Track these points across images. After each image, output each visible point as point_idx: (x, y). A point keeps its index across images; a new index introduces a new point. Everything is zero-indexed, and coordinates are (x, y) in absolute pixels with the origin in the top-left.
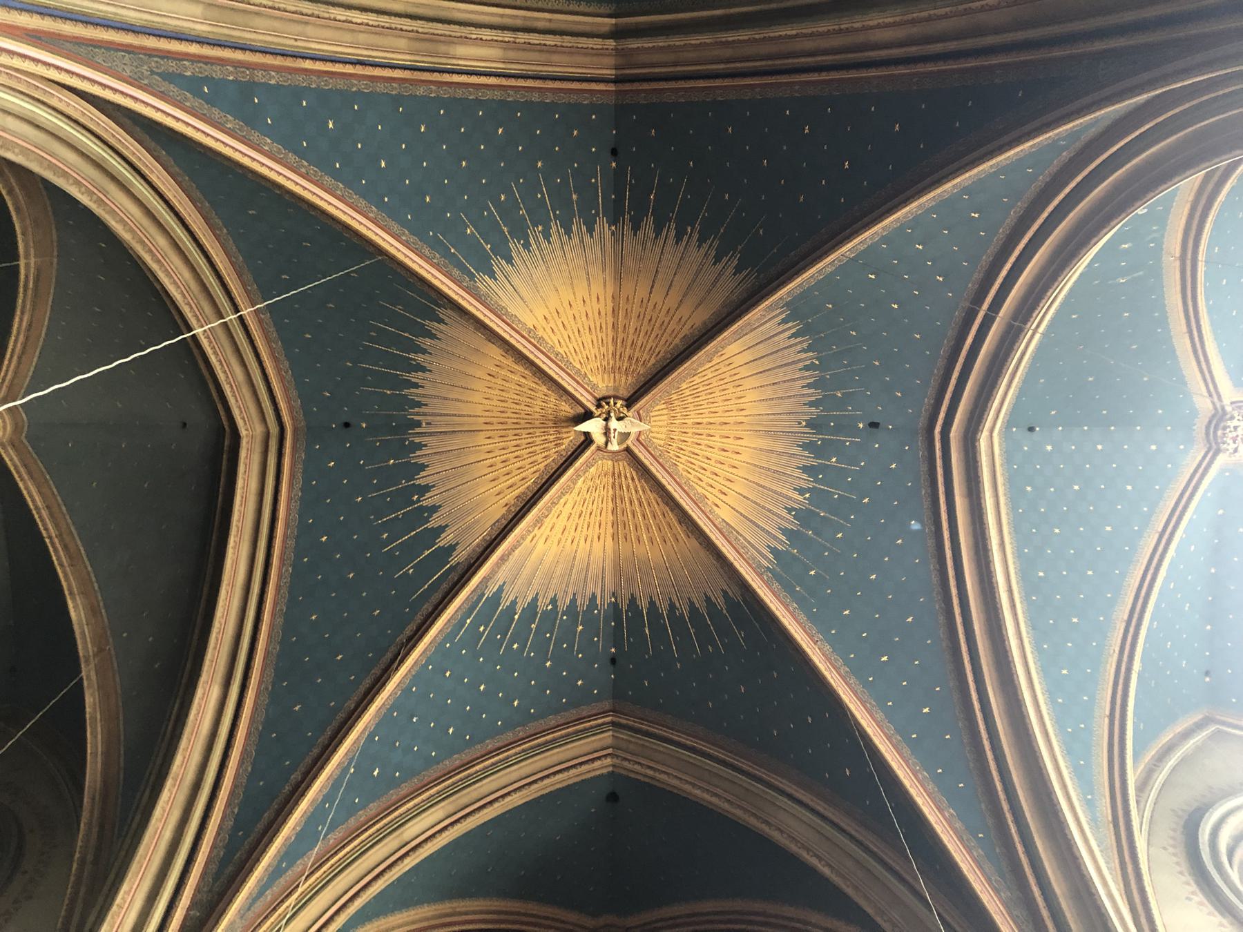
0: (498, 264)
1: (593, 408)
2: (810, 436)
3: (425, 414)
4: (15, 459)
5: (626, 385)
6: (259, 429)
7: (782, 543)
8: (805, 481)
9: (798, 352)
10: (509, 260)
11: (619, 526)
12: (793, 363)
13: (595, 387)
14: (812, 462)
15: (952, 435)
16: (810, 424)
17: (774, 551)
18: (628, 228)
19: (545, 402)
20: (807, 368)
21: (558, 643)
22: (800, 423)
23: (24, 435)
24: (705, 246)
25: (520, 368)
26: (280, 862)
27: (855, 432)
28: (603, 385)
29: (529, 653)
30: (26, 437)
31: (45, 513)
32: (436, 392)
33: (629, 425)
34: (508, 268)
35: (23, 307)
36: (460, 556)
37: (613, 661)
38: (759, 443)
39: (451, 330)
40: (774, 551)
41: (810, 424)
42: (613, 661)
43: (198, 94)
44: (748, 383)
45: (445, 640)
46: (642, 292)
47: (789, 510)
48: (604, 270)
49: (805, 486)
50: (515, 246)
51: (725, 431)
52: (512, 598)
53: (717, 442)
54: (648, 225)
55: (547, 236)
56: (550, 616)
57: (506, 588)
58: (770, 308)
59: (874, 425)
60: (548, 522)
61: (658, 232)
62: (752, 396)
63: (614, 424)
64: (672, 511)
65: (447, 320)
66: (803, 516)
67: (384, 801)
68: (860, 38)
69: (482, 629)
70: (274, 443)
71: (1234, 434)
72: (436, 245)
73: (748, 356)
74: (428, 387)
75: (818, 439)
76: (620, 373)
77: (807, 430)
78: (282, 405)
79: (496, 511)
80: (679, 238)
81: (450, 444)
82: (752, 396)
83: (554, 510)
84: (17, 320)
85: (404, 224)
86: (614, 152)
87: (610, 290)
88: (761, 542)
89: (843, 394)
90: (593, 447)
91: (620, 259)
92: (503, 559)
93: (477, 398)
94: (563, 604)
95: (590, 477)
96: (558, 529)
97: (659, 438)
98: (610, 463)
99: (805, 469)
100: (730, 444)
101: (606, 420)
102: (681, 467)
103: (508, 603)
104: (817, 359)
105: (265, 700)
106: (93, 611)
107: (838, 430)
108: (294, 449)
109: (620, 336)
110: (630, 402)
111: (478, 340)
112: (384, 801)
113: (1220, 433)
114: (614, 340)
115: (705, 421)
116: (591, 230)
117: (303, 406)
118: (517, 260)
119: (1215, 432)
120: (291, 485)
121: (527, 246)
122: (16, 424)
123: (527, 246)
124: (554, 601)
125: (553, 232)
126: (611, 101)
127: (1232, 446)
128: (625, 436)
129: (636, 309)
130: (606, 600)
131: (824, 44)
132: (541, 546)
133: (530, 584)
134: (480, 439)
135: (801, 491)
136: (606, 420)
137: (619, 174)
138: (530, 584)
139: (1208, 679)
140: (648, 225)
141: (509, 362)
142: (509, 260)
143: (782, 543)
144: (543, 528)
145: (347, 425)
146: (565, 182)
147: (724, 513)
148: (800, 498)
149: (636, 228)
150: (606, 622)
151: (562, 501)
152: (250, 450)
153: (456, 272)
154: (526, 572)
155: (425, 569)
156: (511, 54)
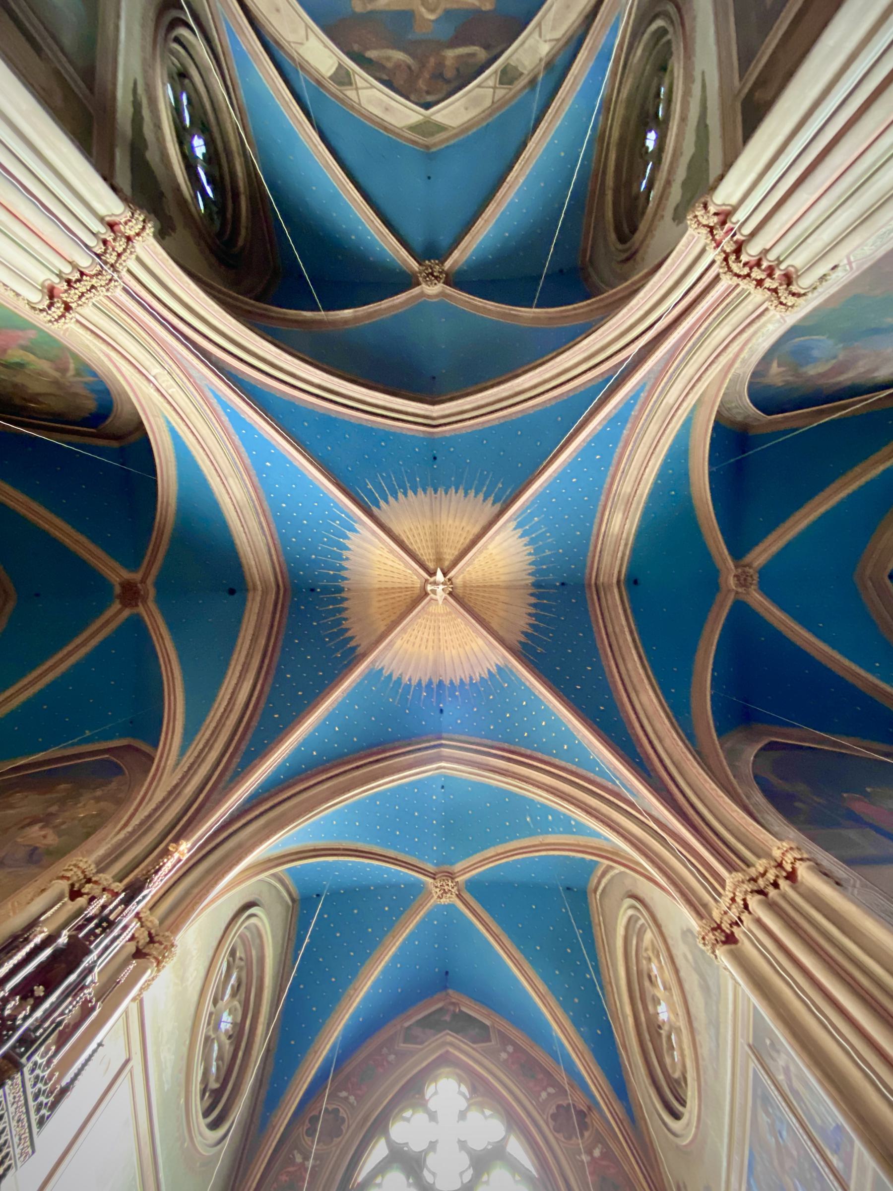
0: (520, 531)
1: (448, 577)
2: (435, 681)
5: (459, 591)
6: (435, 415)
7: (386, 673)
8: (414, 682)
10: (521, 537)
11: (386, 591)
13: (457, 578)
14: (424, 684)
16: (441, 682)
17: (382, 669)
18: (531, 591)
19: (449, 555)
21: (325, 562)
24: (528, 626)
25: (468, 541)
26: (231, 408)
28: (458, 581)
30: (425, 300)
32: (453, 503)
33: (440, 593)
34: (517, 536)
35: (499, 307)
36: (375, 509)
37: (313, 590)
38: (431, 658)
39: (489, 509)
40: (382, 669)
41: (441, 682)
42: (313, 590)
43: (632, 398)
44: (461, 650)
45: (335, 503)
48: (510, 581)
49: (412, 682)
50: (526, 539)
51: (436, 641)
52: (352, 537)
53: (431, 637)
54: (533, 600)
55: (530, 554)
56: (340, 557)
57: (358, 535)
58: (504, 657)
60: (391, 556)
61: (530, 605)
63: (441, 587)
67: (251, 468)
68: (639, 687)
69: (338, 522)
70: (429, 422)
71: (444, 884)
72: (533, 502)
73: (476, 649)
74: (456, 498)
75: (434, 686)
78: (448, 428)
79: (397, 529)
81: (427, 508)
85: (546, 488)
86: (563, 584)
87: (501, 584)
88: (386, 662)
89: (450, 697)
90: (429, 578)
91: (516, 588)
92: (374, 533)
93: (450, 522)
94: (345, 564)
97: (432, 609)
98: (419, 586)
99: (420, 681)
100: (430, 644)
101: (442, 583)
103: (349, 536)
105: (310, 407)
106: (346, 322)
107: (439, 694)
108: (423, 432)
110: (450, 594)
111: (483, 522)
112: (251, 468)
113: (444, 878)
114: (478, 586)
116: (529, 574)
117: (446, 437)
118: (520, 540)
119: (446, 876)
121: (525, 545)
123: (525, 545)
124: (347, 559)
125: (531, 557)
126: (586, 582)
127: (439, 885)
128: (434, 592)
131: (633, 673)
134: (428, 523)
135: (410, 680)
136: (442, 583)
137: (555, 587)
138: (358, 547)
139: (315, 896)
140: (533, 600)
141: (471, 537)
142: (521, 537)
143: (386, 673)
145: (435, 458)
146: (552, 562)
147: (399, 642)
148: (407, 679)
151: (401, 563)
152: (426, 410)
153: (519, 513)
154: (366, 545)
155: (370, 494)
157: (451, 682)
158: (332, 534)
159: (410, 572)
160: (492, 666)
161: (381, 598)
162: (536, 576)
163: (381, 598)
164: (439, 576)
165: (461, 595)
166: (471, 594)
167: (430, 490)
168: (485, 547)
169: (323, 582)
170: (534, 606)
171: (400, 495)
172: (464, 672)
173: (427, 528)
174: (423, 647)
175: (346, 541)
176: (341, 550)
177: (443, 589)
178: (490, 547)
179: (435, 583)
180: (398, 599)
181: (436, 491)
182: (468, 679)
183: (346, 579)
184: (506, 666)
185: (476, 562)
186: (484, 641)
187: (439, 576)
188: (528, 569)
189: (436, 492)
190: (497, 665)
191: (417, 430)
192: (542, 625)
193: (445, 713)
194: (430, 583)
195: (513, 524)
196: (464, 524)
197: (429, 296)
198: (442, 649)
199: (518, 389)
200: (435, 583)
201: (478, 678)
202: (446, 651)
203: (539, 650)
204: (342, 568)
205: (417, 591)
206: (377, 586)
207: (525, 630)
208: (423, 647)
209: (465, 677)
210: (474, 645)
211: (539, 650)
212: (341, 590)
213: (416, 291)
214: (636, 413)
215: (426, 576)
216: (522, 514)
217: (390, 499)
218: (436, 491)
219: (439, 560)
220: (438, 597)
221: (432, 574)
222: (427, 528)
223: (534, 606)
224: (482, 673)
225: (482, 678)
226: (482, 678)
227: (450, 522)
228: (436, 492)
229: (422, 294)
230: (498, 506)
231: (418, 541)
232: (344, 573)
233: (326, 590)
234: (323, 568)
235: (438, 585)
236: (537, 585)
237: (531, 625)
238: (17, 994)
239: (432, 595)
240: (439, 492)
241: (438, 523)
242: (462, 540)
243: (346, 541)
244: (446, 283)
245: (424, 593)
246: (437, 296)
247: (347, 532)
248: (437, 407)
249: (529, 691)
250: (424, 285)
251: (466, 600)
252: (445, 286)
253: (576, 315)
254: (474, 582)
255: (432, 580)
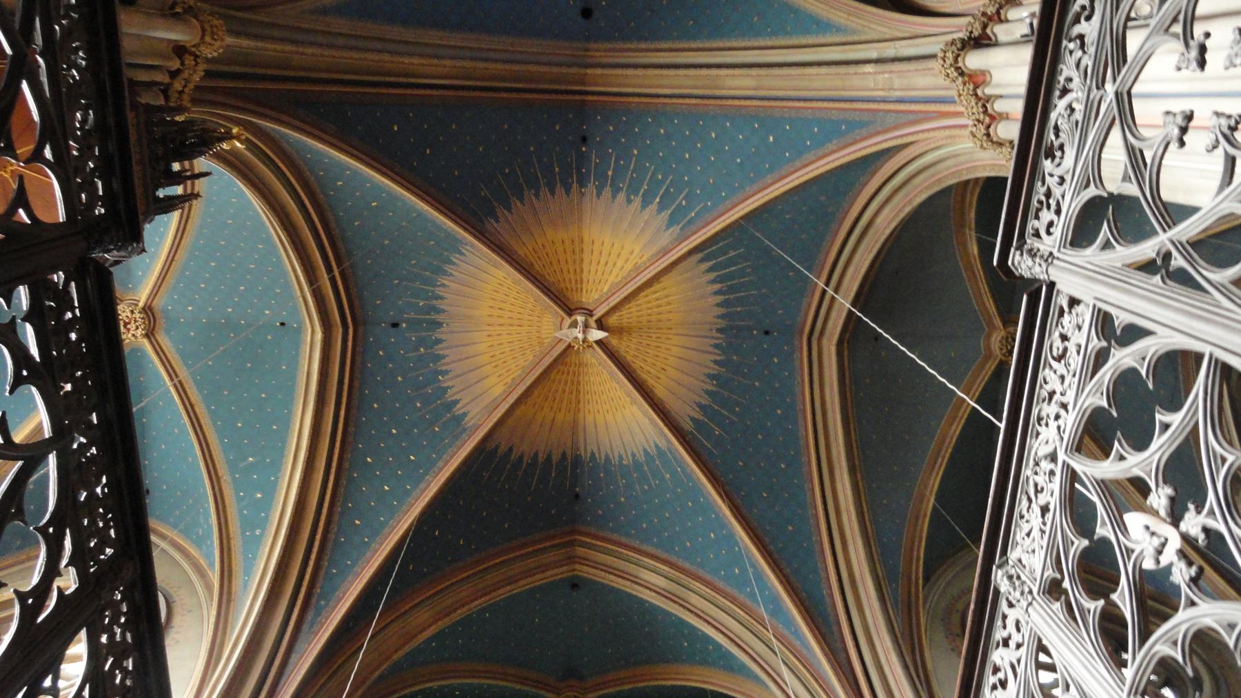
0: (653, 451)
1: (594, 345)
2: (440, 318)
3: (713, 338)
4: (933, 478)
5: (572, 359)
6: (825, 341)
8: (440, 291)
9: (454, 387)
12: (459, 376)
13: (593, 356)
15: (341, 330)
16: (440, 325)
20: (447, 372)
21: (627, 167)
22: (447, 325)
23: (985, 333)
25: (644, 376)
27: (408, 321)
29: (650, 166)
31: (983, 291)
34: (646, 446)
36: (699, 256)
37: (584, 140)
41: (440, 325)
42: (584, 140)
43: (796, 630)
46: (560, 417)
47: (451, 275)
49: (441, 288)
50: (641, 458)
51: (501, 321)
55: (620, 457)
56: (633, 190)
59: (395, 325)
60: (629, 266)
62: (482, 347)
63: (580, 336)
64: (538, 271)
65: (688, 420)
66: (439, 271)
70: (815, 334)
74: (707, 361)
75: (434, 316)
76: (575, 364)
77: (442, 321)
79: (666, 281)
80: (536, 455)
82: (482, 347)
83: (625, 274)
84: (958, 432)
86: (577, 496)
87: (581, 415)
89: (419, 350)
90: (595, 318)
93: (675, 350)
94: (621, 197)
95: (598, 292)
96: (623, 257)
99: (442, 298)
102: (532, 300)
103: (663, 214)
104: (440, 381)
107: (419, 322)
109: (573, 397)
110: (570, 346)
114: (579, 383)
115: (515, 328)
118: (641, 449)
120: (809, 305)
122: (988, 340)
123: (633, 455)
124: (629, 201)
125: (617, 458)
128: (574, 325)
129: (564, 405)
130: (591, 188)
132: (637, 249)
133: (647, 222)
135: (443, 285)
141: (651, 381)
144: (634, 262)
145: (767, 333)
149: (564, 454)
150: (589, 173)
153: (678, 456)
156: (632, 568)
157: (439, 341)
158: (667, 190)
159: (605, 290)
160: (464, 406)
161: (568, 243)
162: (590, 461)
163: (568, 243)
164: (596, 335)
165: (568, 360)
166: (568, 374)
167: (722, 323)
168: (634, 402)
169: (596, 157)
170: (549, 459)
171: (717, 287)
172: (454, 362)
173: (670, 316)
174: (491, 303)
175: (654, 206)
176: (643, 196)
177: (576, 338)
178: (635, 409)
179: (586, 326)
180: (565, 269)
181: (720, 330)
182: (444, 368)
183: (599, 194)
184: (465, 430)
185: (614, 384)
186: (501, 395)
187: (596, 335)
188: (600, 453)
189: (719, 330)
190: (465, 414)
191: (807, 315)
192: (520, 473)
193: (392, 331)
194: (586, 320)
195: (662, 444)
196: (671, 372)
197: (989, 336)
198: (488, 328)
199: (837, 472)
200: (586, 326)
201: (446, 385)
202: (486, 333)
203: (486, 475)
204: (616, 191)
205: (575, 297)
206: (586, 238)
207: (515, 450)
208: (491, 303)
209: (448, 364)
210: (493, 380)
211: (486, 475)
212: (582, 183)
213: (998, 322)
214: (780, 629)
215: (598, 313)
216: (675, 458)
217: (713, 275)
218: (720, 330)
219: (619, 331)
220: (565, 331)
221: (601, 325)
222: (670, 316)
223: (549, 459)
224: (455, 390)
225: (445, 390)
226: (445, 390)
227: (675, 350)
228: (719, 330)
229: (993, 327)
230: (688, 426)
231: (650, 305)
232: (607, 191)
233: (582, 159)
234: (616, 161)
235: (584, 332)
236: (577, 461)
237: (521, 458)
238: (157, 199)
239: (568, 321)
240: (719, 335)
241: (674, 331)
242: (646, 368)
243: (654, 206)
244: (1001, 360)
245: (573, 308)
246: (988, 347)
247: (669, 212)
248: (833, 349)
249: (430, 466)
250: (1003, 333)
251: (561, 368)
252: (997, 362)
253: (911, 559)
254: (587, 379)
255: (592, 322)
